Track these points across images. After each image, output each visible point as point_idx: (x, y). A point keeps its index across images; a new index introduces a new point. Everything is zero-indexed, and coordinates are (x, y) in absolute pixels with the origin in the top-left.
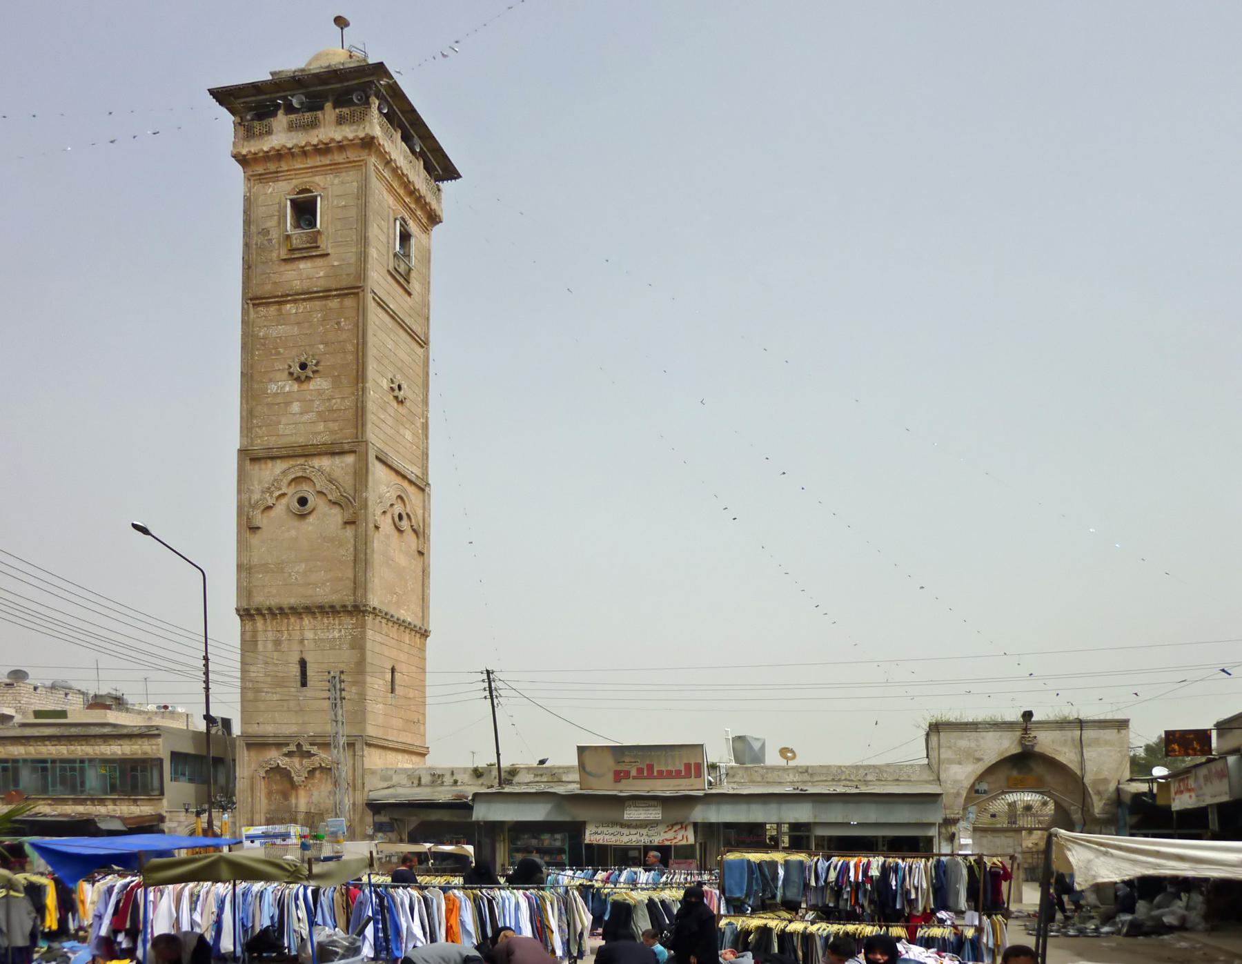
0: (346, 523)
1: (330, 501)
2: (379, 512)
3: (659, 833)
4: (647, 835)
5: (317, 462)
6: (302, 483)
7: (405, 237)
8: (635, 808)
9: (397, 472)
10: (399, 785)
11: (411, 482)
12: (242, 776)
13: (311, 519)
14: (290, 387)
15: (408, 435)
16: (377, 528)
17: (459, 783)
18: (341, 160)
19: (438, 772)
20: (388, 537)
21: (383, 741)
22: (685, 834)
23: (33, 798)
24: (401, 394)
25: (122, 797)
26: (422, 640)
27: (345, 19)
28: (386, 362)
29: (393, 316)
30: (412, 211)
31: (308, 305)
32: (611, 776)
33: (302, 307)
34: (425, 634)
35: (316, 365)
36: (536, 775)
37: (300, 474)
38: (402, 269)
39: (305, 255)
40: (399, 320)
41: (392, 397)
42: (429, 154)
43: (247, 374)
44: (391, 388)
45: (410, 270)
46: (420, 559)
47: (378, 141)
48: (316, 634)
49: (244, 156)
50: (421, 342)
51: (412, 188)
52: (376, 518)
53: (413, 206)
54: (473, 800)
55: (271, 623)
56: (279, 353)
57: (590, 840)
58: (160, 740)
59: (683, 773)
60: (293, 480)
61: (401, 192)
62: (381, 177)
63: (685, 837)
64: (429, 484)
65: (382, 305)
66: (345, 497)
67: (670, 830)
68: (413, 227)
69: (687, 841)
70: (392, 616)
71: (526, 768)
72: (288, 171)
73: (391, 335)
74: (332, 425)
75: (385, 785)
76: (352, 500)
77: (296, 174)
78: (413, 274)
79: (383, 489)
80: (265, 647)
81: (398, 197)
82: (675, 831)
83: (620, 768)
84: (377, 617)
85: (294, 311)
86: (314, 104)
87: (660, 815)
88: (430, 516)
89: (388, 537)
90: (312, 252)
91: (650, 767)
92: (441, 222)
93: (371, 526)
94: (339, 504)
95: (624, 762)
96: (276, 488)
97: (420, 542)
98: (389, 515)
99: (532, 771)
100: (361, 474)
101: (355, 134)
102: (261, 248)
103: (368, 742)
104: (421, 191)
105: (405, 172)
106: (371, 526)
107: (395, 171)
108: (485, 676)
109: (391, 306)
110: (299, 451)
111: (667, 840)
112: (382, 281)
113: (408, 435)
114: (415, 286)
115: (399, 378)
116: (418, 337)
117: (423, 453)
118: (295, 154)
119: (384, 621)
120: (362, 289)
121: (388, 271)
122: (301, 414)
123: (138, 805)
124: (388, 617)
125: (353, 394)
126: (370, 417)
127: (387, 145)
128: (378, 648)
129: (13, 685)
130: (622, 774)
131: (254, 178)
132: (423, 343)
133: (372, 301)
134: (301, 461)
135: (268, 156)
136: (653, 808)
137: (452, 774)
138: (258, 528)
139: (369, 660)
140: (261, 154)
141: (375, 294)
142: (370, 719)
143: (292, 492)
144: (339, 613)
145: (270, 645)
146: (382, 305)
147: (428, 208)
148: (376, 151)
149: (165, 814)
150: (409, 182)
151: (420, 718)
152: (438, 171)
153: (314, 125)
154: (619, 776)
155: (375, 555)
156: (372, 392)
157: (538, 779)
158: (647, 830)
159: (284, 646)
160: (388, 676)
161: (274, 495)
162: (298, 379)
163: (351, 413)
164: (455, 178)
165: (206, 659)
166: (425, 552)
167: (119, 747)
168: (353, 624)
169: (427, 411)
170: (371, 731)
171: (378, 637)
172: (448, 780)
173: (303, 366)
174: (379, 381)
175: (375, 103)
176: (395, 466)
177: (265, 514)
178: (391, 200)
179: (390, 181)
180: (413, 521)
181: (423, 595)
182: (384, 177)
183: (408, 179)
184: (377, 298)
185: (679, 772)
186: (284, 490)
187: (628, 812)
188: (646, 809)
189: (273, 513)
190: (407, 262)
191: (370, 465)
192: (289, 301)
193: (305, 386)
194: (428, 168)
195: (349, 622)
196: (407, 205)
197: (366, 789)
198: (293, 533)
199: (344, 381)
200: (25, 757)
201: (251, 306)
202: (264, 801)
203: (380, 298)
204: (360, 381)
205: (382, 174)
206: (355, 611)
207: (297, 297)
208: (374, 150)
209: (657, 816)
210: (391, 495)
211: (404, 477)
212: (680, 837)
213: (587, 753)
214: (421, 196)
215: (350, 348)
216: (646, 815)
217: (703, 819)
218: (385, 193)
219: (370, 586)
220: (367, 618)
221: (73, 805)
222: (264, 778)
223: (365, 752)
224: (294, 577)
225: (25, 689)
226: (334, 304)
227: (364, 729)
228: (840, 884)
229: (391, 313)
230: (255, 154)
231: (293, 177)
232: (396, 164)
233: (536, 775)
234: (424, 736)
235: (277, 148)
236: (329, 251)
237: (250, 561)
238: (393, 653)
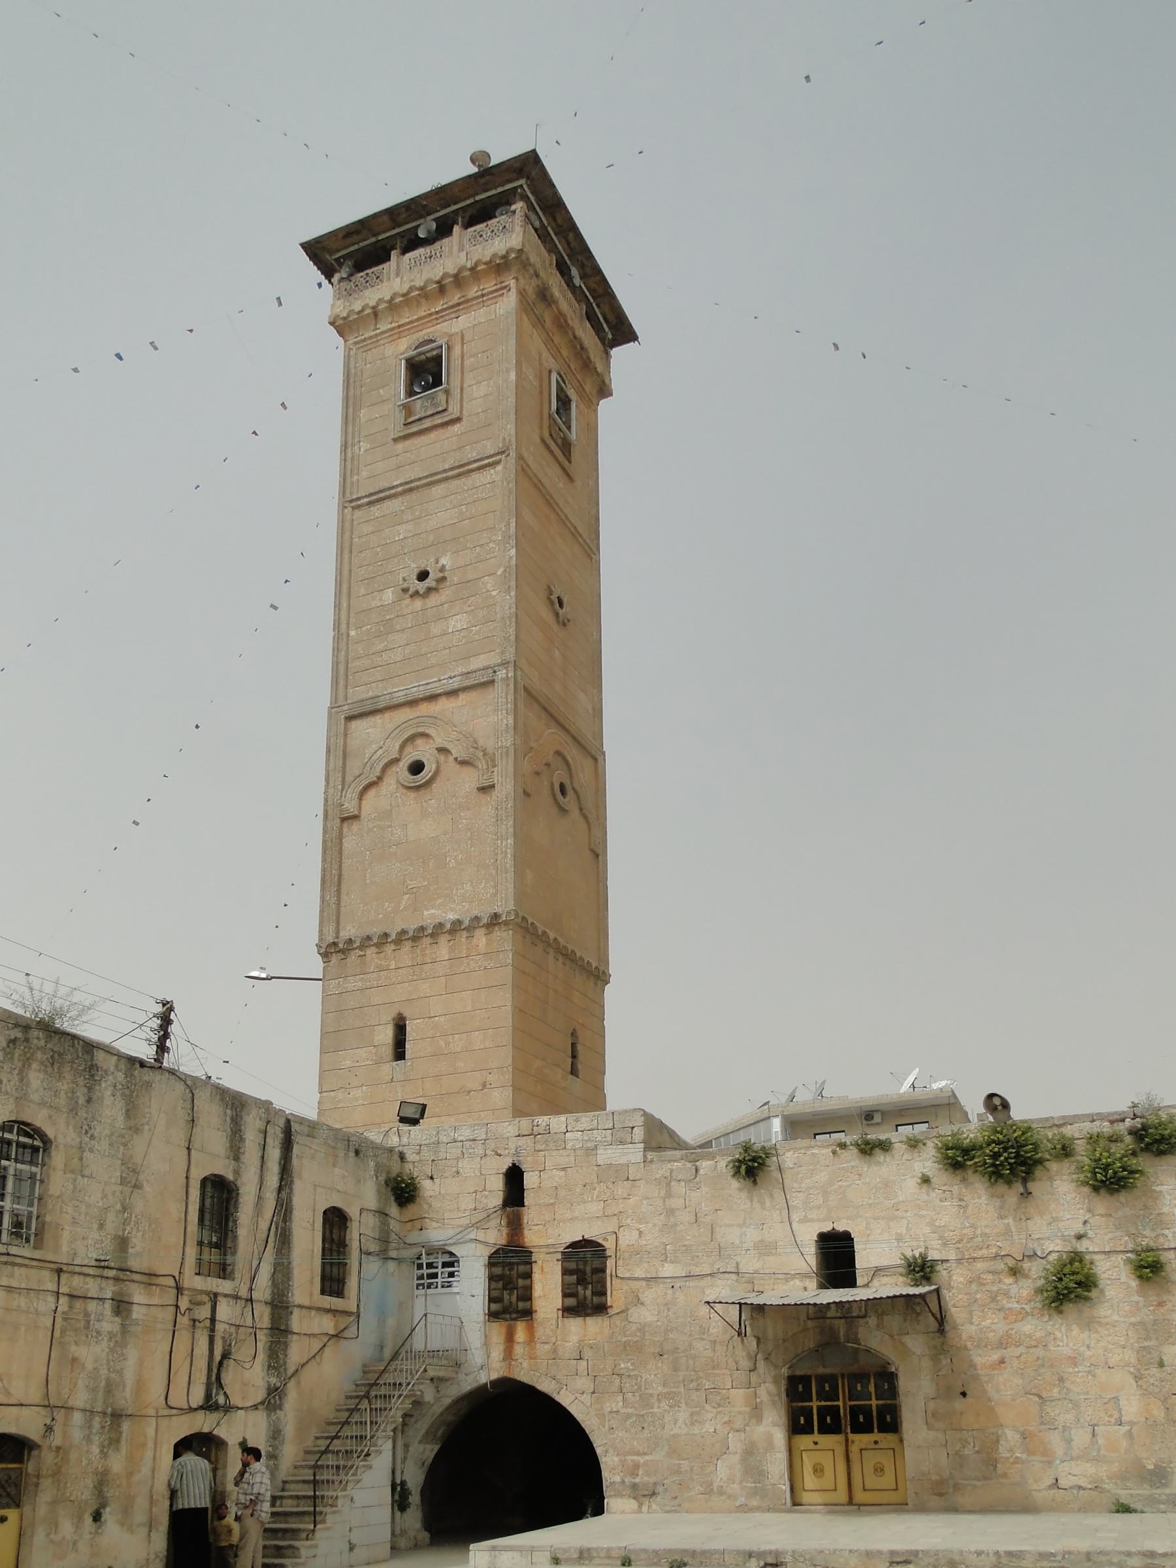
150: (421, 289)
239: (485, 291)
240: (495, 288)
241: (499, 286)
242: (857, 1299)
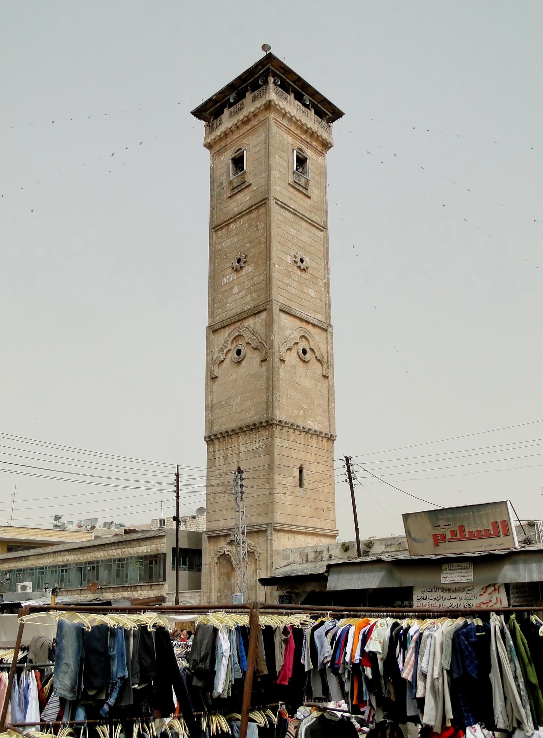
0: (262, 361)
1: (253, 347)
2: (283, 349)
3: (475, 597)
4: (466, 599)
5: (246, 323)
6: (238, 340)
7: (301, 161)
8: (451, 571)
9: (301, 320)
10: (294, 563)
11: (314, 325)
12: (205, 563)
13: (244, 364)
14: (233, 277)
15: (312, 293)
16: (283, 361)
17: (333, 558)
18: (256, 123)
19: (319, 549)
20: (294, 367)
21: (290, 527)
22: (499, 596)
23: (104, 588)
24: (303, 266)
25: (145, 584)
26: (330, 443)
27: (267, 45)
28: (289, 244)
29: (295, 213)
30: (309, 143)
31: (241, 221)
32: (431, 541)
33: (238, 223)
34: (331, 439)
35: (245, 258)
36: (387, 546)
37: (237, 334)
38: (303, 182)
39: (239, 190)
40: (299, 215)
41: (296, 267)
42: (319, 105)
43: (211, 276)
44: (294, 261)
45: (308, 181)
46: (325, 382)
47: (274, 103)
48: (246, 447)
49: (210, 143)
50: (320, 227)
51: (306, 128)
52: (281, 353)
53: (309, 140)
54: (327, 571)
55: (223, 444)
56: (227, 257)
57: (418, 606)
58: (164, 540)
59: (492, 533)
60: (234, 339)
61: (298, 132)
62: (280, 125)
63: (499, 600)
64: (331, 326)
65: (284, 207)
66: (261, 343)
67: (484, 592)
68: (309, 153)
69: (501, 604)
70: (298, 426)
71: (379, 540)
72: (231, 142)
73: (294, 226)
74: (255, 295)
75: (285, 563)
76: (265, 344)
77: (235, 143)
78: (311, 183)
79: (288, 332)
80: (219, 462)
81: (295, 136)
82: (490, 594)
83: (437, 532)
84: (285, 428)
85: (234, 228)
86: (241, 96)
87: (472, 577)
88: (332, 349)
89: (294, 367)
90: (242, 187)
91: (462, 528)
92: (332, 146)
93: (277, 360)
94: (258, 349)
95: (439, 526)
96: (225, 347)
97: (324, 368)
98: (294, 351)
99: (383, 542)
100: (269, 324)
101: (260, 104)
102: (219, 195)
103: (275, 528)
104: (313, 129)
105: (298, 118)
106: (277, 360)
107: (291, 119)
108: (344, 463)
109: (291, 206)
110: (237, 318)
111: (484, 603)
112: (284, 191)
113: (312, 293)
114: (313, 190)
115: (301, 254)
116: (318, 224)
117: (326, 304)
118: (233, 131)
119: (291, 431)
120: (268, 199)
121: (289, 184)
122: (238, 293)
123: (152, 590)
124: (295, 428)
125: (265, 270)
126: (274, 282)
127: (282, 104)
128: (285, 452)
129: (195, 517)
130: (439, 538)
131: (215, 155)
132: (323, 228)
133: (275, 205)
134: (238, 324)
135: (220, 138)
136: (466, 570)
137: (328, 550)
138: (217, 377)
139: (277, 461)
140: (217, 139)
141: (278, 200)
142: (278, 508)
143: (233, 347)
144: (258, 428)
145: (222, 460)
146: (284, 207)
147: (320, 139)
148: (274, 109)
149: (165, 596)
150: (302, 124)
151: (330, 506)
152: (329, 115)
153: (241, 109)
154: (439, 540)
155: (281, 382)
156: (277, 266)
157: (388, 549)
158: (464, 593)
159: (229, 460)
160: (297, 473)
161: (224, 352)
162: (236, 270)
163: (263, 284)
164: (341, 117)
165: (177, 475)
166: (329, 375)
167: (145, 547)
168: (266, 435)
169: (328, 274)
170: (280, 518)
171: (286, 444)
172: (325, 555)
173: (239, 261)
174: (284, 258)
175: (271, 79)
176: (298, 315)
177: (220, 367)
178: (290, 139)
179: (288, 127)
180: (317, 353)
181: (329, 408)
182: (283, 125)
183: (301, 122)
184: (279, 203)
185: (488, 531)
186: (229, 347)
187: (444, 575)
188: (460, 571)
189: (224, 365)
190: (306, 177)
191: (275, 316)
192: (232, 222)
193: (240, 274)
194: (319, 113)
195: (264, 433)
196: (304, 140)
197: (274, 568)
198: (234, 376)
199: (260, 263)
200: (102, 559)
201: (214, 232)
202: (217, 582)
203: (282, 203)
204: (268, 259)
205: (281, 124)
206: (268, 425)
207: (236, 218)
208: (272, 109)
209: (469, 578)
210: (297, 336)
211: (308, 322)
212: (494, 601)
213: (410, 520)
214: (313, 132)
215: (263, 240)
216: (459, 578)
217: (511, 579)
218: (285, 136)
219: (276, 404)
220: (274, 429)
221: (122, 591)
222: (217, 563)
223: (274, 537)
224: (234, 408)
225: (201, 519)
226: (254, 215)
227: (273, 518)
228: (336, 666)
229: (292, 211)
230: (214, 139)
231: (233, 145)
232: (290, 115)
233: (387, 546)
234: (334, 520)
235: (224, 131)
236: (251, 182)
237: (212, 401)
238: (301, 455)
239: (317, 148)
240: (320, 150)
241: (321, 151)
242: (282, 664)
